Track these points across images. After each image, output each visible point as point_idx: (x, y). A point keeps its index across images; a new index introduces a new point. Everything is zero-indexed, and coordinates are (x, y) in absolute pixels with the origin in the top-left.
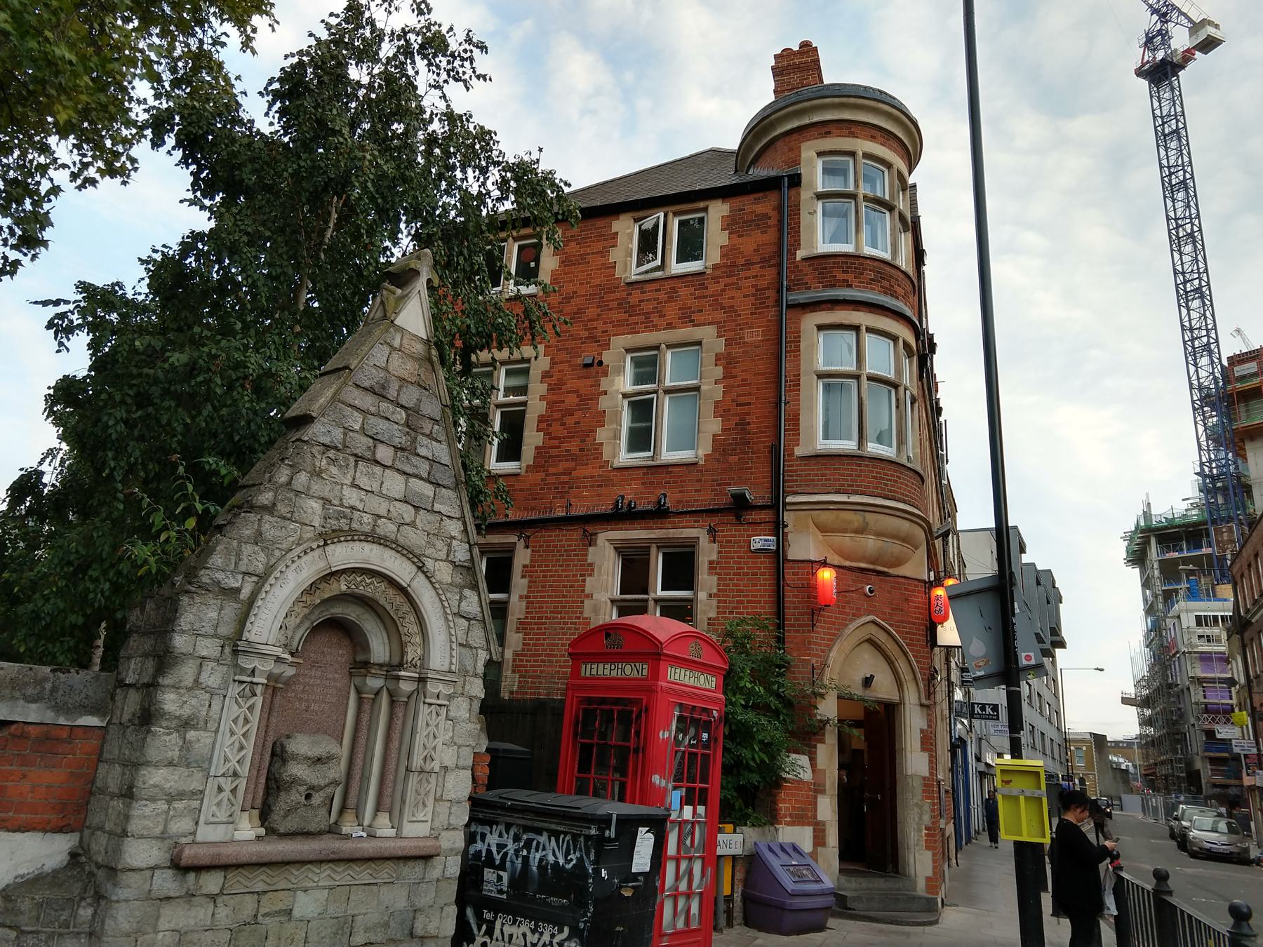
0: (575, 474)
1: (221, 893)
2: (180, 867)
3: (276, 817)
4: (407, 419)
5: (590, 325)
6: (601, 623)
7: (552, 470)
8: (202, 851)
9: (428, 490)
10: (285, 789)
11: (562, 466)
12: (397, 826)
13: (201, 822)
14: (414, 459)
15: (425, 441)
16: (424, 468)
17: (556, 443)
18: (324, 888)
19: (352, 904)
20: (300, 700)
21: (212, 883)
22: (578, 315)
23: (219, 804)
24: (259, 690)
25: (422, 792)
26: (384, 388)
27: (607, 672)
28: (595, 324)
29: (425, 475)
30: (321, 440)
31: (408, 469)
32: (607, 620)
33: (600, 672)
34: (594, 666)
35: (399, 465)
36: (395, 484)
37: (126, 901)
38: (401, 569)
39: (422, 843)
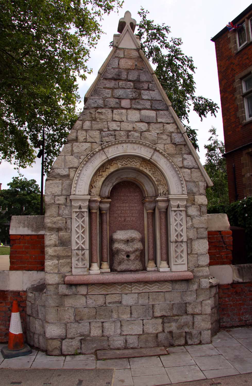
1: (87, 294)
2: (70, 285)
3: (115, 264)
4: (134, 85)
9: (152, 114)
10: (116, 254)
13: (73, 267)
14: (141, 102)
15: (147, 92)
16: (148, 105)
18: (135, 293)
19: (151, 300)
20: (121, 217)
21: (83, 290)
23: (78, 260)
25: (179, 251)
26: (119, 76)
29: (149, 107)
30: (93, 106)
31: (139, 107)
35: (134, 106)
36: (134, 115)
38: (145, 153)
39: (181, 274)
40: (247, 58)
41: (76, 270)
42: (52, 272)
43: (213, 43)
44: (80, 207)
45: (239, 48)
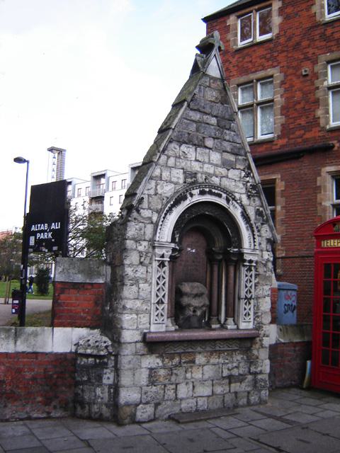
0: (305, 137)
4: (218, 124)
5: (305, 51)
6: (328, 220)
7: (292, 136)
8: (154, 335)
9: (232, 158)
11: (298, 133)
12: (236, 323)
17: (292, 120)
22: (297, 46)
24: (166, 264)
27: (336, 244)
28: (308, 50)
32: (331, 218)
33: (332, 244)
34: (329, 241)
36: (216, 157)
37: (127, 355)
40: (251, 62)
41: (245, 324)
42: (130, 328)
43: (204, 25)
44: (163, 256)
45: (241, 44)
